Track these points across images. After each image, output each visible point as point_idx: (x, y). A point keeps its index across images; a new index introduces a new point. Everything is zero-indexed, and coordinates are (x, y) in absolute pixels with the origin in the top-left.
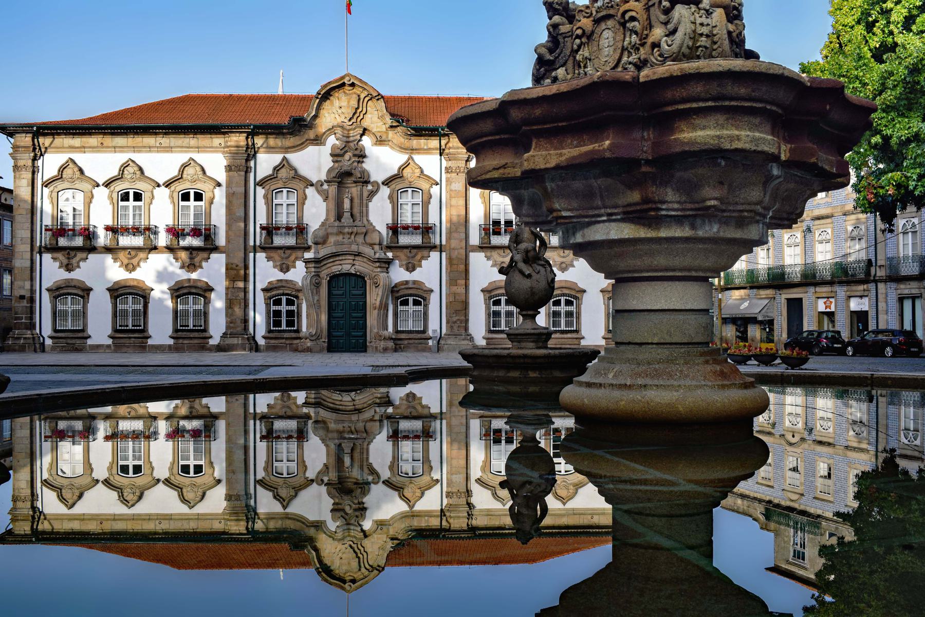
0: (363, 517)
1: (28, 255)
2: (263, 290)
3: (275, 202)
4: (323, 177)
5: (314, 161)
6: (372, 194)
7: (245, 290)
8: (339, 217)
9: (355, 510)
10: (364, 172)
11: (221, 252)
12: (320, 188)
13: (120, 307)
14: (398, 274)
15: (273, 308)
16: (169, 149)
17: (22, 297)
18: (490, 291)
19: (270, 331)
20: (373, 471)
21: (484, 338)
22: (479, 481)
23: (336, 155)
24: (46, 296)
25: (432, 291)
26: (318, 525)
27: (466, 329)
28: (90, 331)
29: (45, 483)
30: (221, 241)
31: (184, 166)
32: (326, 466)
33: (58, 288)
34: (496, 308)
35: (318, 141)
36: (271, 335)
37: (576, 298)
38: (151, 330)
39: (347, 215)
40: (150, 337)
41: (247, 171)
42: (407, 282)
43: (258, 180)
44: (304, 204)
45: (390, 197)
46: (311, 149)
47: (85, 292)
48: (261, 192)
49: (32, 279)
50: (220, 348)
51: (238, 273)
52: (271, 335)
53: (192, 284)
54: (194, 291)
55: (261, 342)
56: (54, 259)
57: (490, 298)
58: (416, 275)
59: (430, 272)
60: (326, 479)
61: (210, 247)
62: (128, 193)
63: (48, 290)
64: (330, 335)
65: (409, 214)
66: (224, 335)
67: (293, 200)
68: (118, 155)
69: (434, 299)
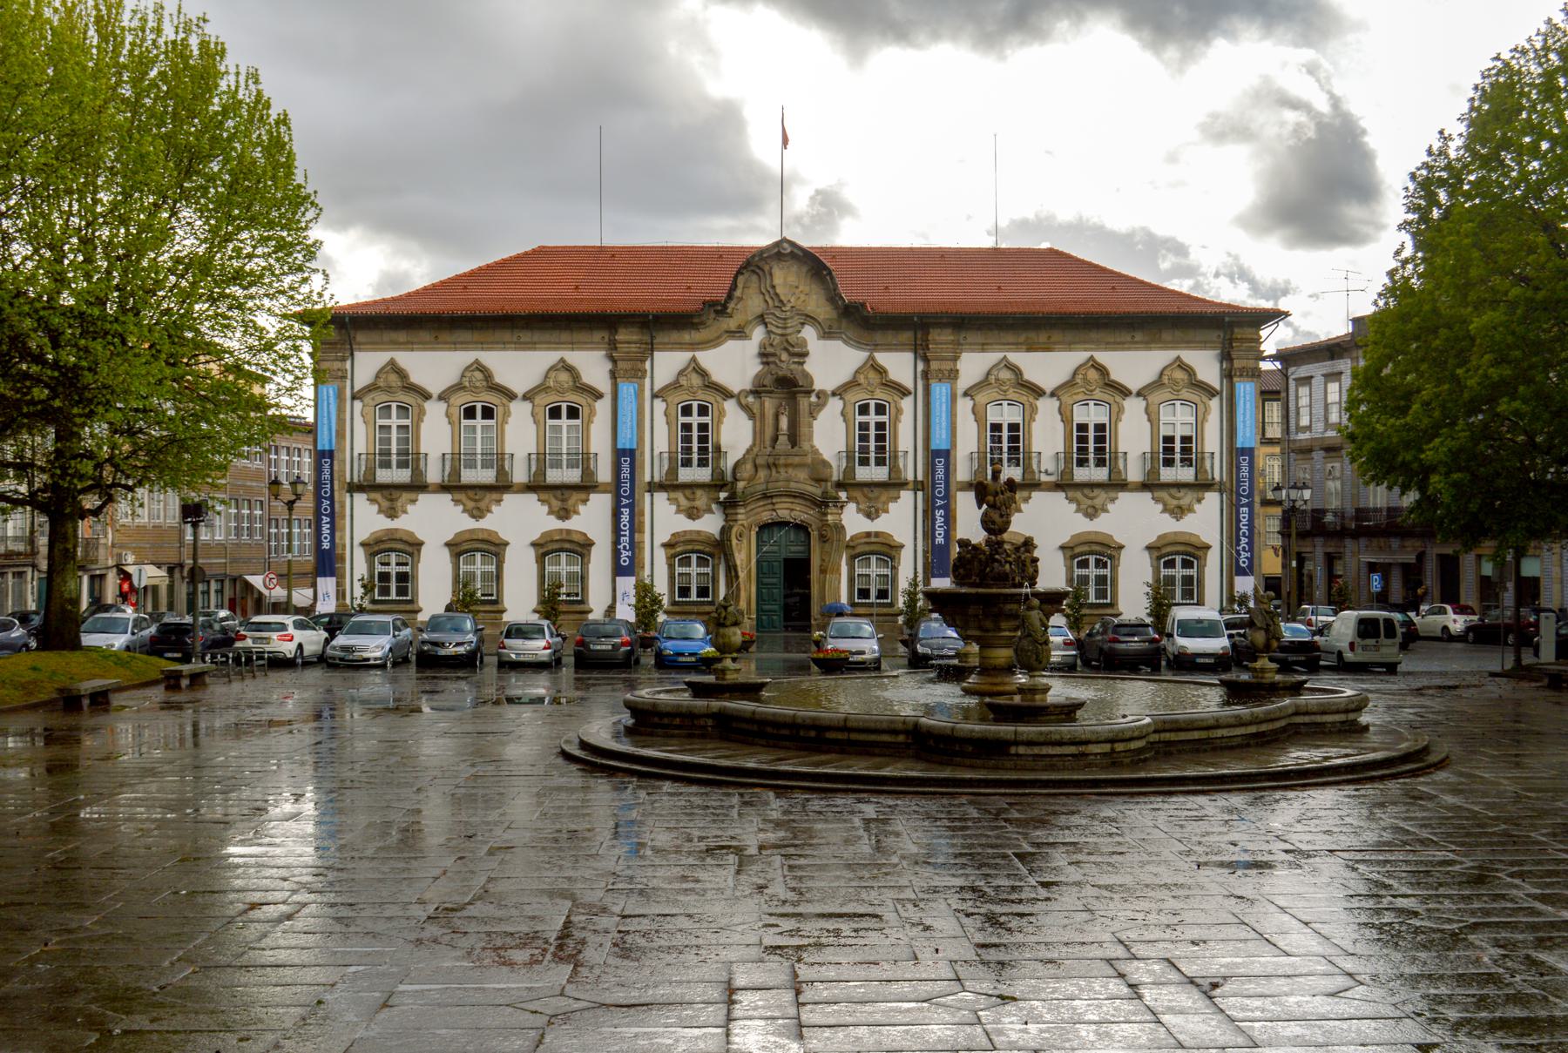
0: (762, 346)
2: (665, 545)
5: (734, 362)
6: (821, 406)
9: (773, 355)
10: (807, 376)
15: (1078, 572)
16: (531, 346)
19: (674, 603)
20: (746, 408)
22: (598, 396)
23: (765, 355)
24: (360, 554)
25: (1208, 547)
26: (827, 334)
29: (1211, 392)
32: (813, 415)
33: (378, 541)
35: (740, 333)
36: (676, 609)
37: (1111, 557)
38: (508, 601)
39: (783, 439)
42: (868, 534)
46: (731, 345)
47: (411, 547)
52: (676, 609)
53: (564, 536)
54: (567, 546)
56: (371, 501)
57: (1159, 558)
60: (813, 399)
61: (587, 487)
63: (363, 544)
64: (759, 610)
68: (458, 353)
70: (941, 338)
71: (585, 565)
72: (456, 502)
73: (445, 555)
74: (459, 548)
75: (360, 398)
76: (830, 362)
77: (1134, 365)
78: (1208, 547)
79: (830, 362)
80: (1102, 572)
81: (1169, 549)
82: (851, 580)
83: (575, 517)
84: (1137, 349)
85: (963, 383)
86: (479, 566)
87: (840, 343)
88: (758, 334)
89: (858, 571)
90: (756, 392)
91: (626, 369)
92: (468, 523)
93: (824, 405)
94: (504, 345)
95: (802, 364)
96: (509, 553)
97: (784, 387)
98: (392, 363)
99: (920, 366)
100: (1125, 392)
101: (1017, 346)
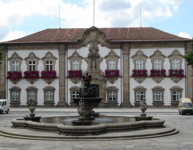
1: (4, 80)
2: (70, 89)
3: (73, 64)
4: (87, 56)
5: (84, 52)
6: (101, 61)
7: (65, 89)
8: (92, 68)
10: (98, 54)
11: (58, 78)
12: (86, 60)
13: (29, 94)
14: (109, 85)
15: (173, 94)
17: (2, 92)
18: (154, 90)
21: (134, 103)
23: (90, 50)
25: (183, 89)
26: (103, 46)
27: (129, 101)
28: (164, 102)
30: (58, 75)
31: (47, 54)
34: (175, 94)
35: (85, 46)
38: (21, 101)
39: (94, 67)
40: (164, 103)
41: (65, 55)
42: (111, 87)
43: (8, 58)
44: (81, 64)
45: (106, 62)
46: (83, 48)
48: (69, 61)
49: (5, 86)
50: (58, 106)
51: (63, 86)
55: (69, 104)
57: (172, 92)
58: (114, 85)
59: (118, 84)
60: (100, 59)
62: (31, 62)
63: (9, 89)
65: (76, 68)
66: (59, 103)
67: (115, 63)
69: (119, 92)
70: (126, 47)
71: (54, 93)
72: (28, 81)
73: (151, 92)
74: (28, 90)
75: (9, 60)
76: (103, 51)
77: (167, 51)
78: (183, 89)
79: (103, 51)
80: (142, 94)
81: (174, 90)
82: (108, 96)
83: (52, 84)
84: (150, 48)
85: (131, 56)
86: (32, 93)
87: (105, 47)
88: (89, 46)
89: (109, 95)
90: (89, 57)
91: (63, 54)
92: (47, 85)
93: (102, 60)
94: (178, 48)
95: (97, 52)
96: (38, 92)
97: (94, 57)
98: (15, 53)
99: (122, 52)
100: (147, 57)
101: (50, 49)
